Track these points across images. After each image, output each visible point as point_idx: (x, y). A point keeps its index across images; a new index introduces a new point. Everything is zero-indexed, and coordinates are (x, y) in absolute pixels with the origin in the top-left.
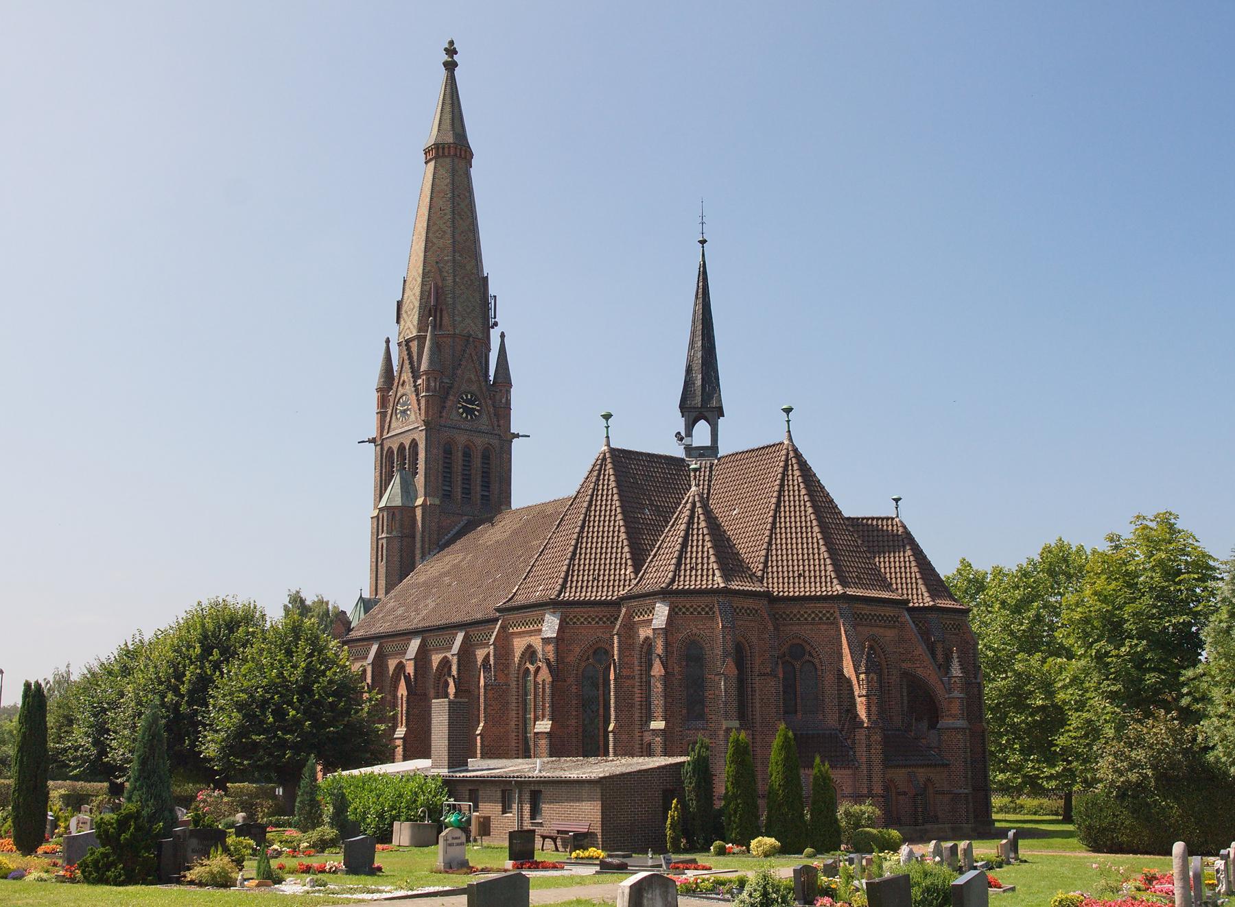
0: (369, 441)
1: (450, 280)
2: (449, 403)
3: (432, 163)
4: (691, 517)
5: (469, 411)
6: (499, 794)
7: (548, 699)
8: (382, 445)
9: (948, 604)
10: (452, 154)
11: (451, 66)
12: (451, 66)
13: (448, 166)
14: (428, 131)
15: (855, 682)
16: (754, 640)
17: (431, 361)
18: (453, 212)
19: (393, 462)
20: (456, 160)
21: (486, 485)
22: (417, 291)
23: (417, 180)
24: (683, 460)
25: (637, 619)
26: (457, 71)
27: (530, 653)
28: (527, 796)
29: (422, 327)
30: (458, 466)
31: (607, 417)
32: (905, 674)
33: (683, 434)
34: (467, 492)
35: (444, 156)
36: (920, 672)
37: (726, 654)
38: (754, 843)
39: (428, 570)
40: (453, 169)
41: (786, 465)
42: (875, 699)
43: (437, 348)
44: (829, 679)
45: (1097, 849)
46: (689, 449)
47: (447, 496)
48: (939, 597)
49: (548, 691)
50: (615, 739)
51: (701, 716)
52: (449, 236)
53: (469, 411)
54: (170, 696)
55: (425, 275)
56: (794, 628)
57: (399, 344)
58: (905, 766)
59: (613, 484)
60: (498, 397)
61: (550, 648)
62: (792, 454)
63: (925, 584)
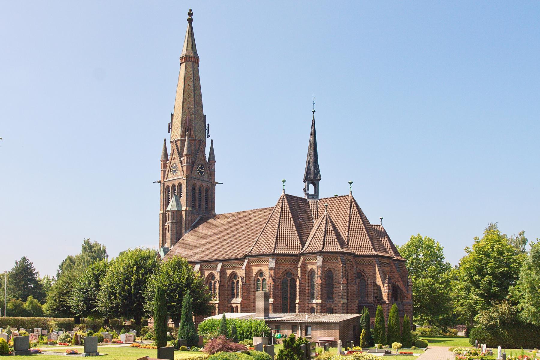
0: (158, 182)
1: (193, 116)
2: (194, 169)
3: (184, 64)
4: (326, 224)
6: (290, 327)
8: (164, 184)
9: (400, 258)
11: (190, 21)
12: (190, 21)
13: (191, 66)
18: (194, 87)
19: (169, 191)
25: (307, 262)
27: (261, 273)
28: (304, 328)
29: (183, 135)
30: (197, 195)
31: (284, 181)
34: (200, 205)
37: (343, 276)
38: (393, 345)
39: (190, 237)
40: (193, 68)
41: (351, 205)
44: (370, 285)
46: (308, 195)
47: (193, 207)
50: (299, 306)
51: (331, 298)
52: (192, 96)
54: (127, 287)
55: (183, 113)
57: (171, 142)
61: (272, 271)
62: (353, 200)
63: (393, 251)
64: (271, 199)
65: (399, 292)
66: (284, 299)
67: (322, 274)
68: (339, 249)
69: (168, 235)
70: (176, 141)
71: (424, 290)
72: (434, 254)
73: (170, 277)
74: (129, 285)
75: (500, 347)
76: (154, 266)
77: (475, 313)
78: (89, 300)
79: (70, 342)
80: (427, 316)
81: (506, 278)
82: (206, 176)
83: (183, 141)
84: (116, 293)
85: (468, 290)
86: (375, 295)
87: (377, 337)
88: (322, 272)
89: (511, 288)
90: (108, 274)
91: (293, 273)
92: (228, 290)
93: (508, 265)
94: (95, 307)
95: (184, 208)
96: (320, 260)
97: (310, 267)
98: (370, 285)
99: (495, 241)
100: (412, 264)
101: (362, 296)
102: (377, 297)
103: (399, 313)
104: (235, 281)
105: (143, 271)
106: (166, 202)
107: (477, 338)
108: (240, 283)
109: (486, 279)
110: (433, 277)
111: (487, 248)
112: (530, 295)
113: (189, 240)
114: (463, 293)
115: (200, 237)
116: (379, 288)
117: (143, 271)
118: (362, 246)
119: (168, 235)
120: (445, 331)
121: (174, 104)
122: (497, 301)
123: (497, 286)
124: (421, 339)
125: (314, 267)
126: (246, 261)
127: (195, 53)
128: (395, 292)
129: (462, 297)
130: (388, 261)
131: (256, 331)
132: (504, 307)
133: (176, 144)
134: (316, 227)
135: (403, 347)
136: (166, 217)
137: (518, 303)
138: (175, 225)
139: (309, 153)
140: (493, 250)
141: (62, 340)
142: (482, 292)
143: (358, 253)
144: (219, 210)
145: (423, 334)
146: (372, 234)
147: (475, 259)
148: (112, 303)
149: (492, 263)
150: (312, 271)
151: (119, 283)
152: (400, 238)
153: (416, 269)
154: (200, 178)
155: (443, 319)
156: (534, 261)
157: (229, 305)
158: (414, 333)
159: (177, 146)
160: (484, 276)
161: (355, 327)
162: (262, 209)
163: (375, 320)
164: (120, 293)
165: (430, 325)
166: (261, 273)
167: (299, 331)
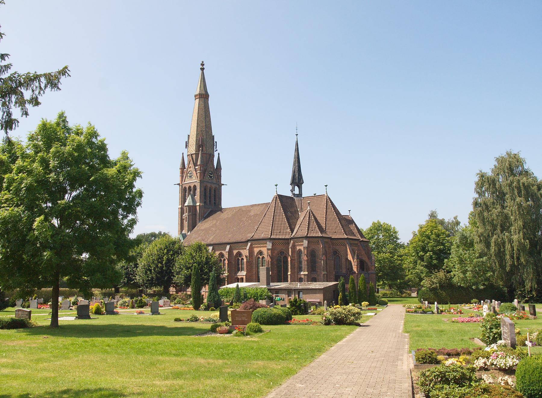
1: (205, 137)
4: (309, 216)
5: (211, 177)
9: (365, 240)
11: (202, 69)
12: (202, 69)
17: (201, 161)
19: (186, 191)
21: (215, 199)
22: (195, 139)
23: (193, 106)
28: (297, 293)
29: (197, 150)
30: (208, 194)
31: (276, 185)
34: (210, 201)
37: (323, 254)
38: (362, 303)
39: (202, 226)
44: (343, 260)
47: (205, 203)
52: (204, 122)
53: (211, 177)
54: (160, 265)
61: (270, 251)
64: (268, 197)
65: (365, 264)
66: (279, 271)
67: (307, 253)
68: (320, 235)
69: (186, 224)
70: (192, 155)
71: (384, 262)
72: (390, 234)
73: (193, 257)
74: (161, 263)
75: (436, 303)
76: (180, 249)
77: (421, 279)
78: (129, 274)
79: (128, 306)
80: (387, 281)
81: (442, 254)
82: (215, 179)
83: (197, 155)
84: (151, 270)
85: (415, 262)
86: (348, 268)
87: (350, 298)
88: (307, 251)
89: (446, 260)
90: (144, 255)
91: (285, 253)
92: (235, 264)
93: (443, 244)
94: (134, 280)
95: (198, 204)
96: (305, 243)
97: (298, 248)
98: (343, 260)
99: (433, 227)
100: (374, 243)
101: (339, 270)
102: (348, 269)
103: (366, 281)
104: (240, 258)
105: (171, 253)
106: (184, 200)
107: (423, 297)
108: (245, 260)
109: (428, 254)
110: (391, 253)
111: (428, 232)
112: (459, 266)
113: (203, 228)
114: (411, 265)
115: (211, 225)
116: (350, 262)
117: (171, 253)
118: (336, 232)
119: (186, 224)
120: (402, 293)
121: (190, 127)
122: (436, 271)
123: (436, 259)
124: (383, 299)
125: (302, 248)
126: (249, 244)
127: (206, 92)
128: (362, 265)
129: (412, 268)
130: (356, 242)
131: (261, 296)
132: (441, 274)
133: (192, 157)
134: (301, 218)
135: (370, 305)
136: (184, 210)
137: (451, 271)
139: (294, 164)
140: (432, 234)
141: (122, 305)
142: (425, 264)
143: (334, 237)
144: (224, 204)
145: (385, 295)
146: (343, 222)
147: (419, 240)
148: (148, 277)
149: (432, 243)
150: (300, 251)
151: (153, 262)
152: (364, 224)
153: (378, 247)
154: (210, 181)
155: (401, 283)
156: (460, 242)
157: (236, 277)
158: (377, 295)
159: (192, 159)
160: (426, 253)
161: (334, 291)
162: (259, 205)
163: (349, 286)
164: (154, 269)
165: (390, 288)
166: (261, 253)
167: (293, 296)
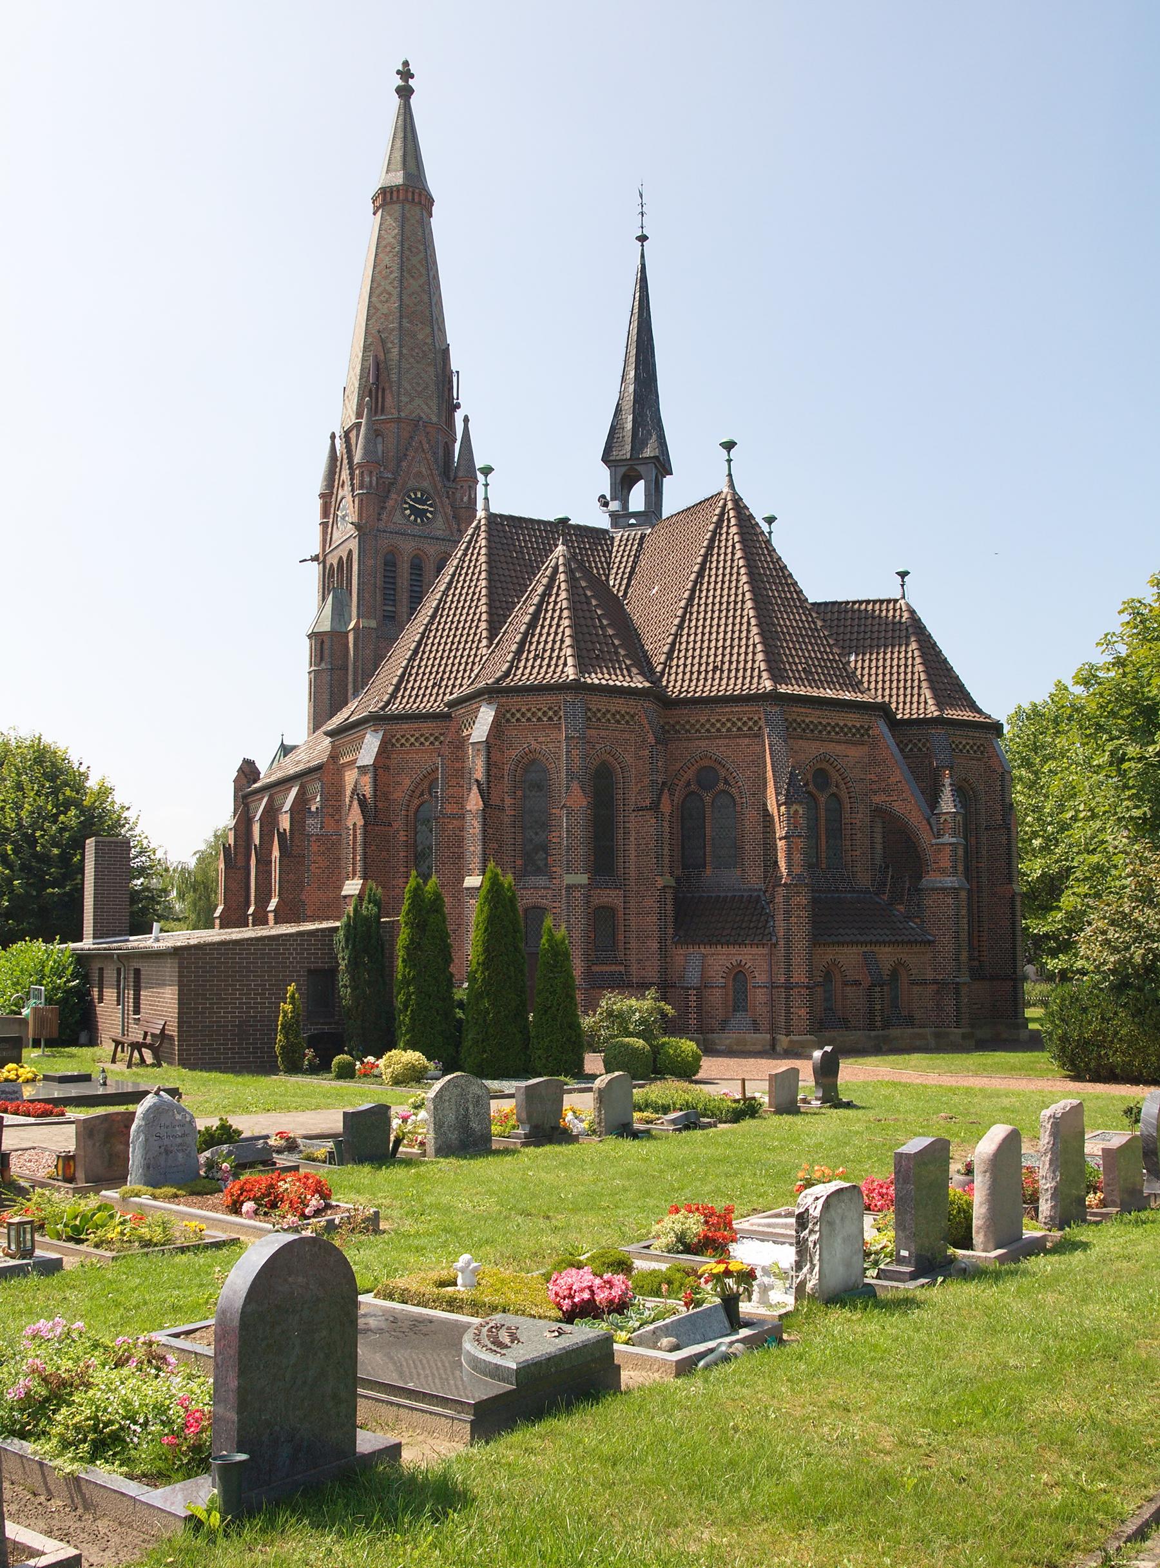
0: (312, 559)
4: (549, 587)
7: (359, 849)
8: (324, 562)
10: (407, 202)
11: (405, 92)
12: (405, 92)
13: (397, 214)
14: (376, 170)
15: (776, 819)
16: (629, 759)
18: (402, 270)
19: (334, 580)
20: (407, 206)
23: (360, 234)
24: (607, 531)
26: (414, 100)
32: (879, 812)
33: (608, 498)
35: (392, 202)
36: (898, 807)
42: (800, 843)
43: (375, 433)
44: (751, 816)
45: (1077, 1077)
46: (617, 519)
48: (952, 706)
49: (359, 838)
52: (395, 298)
56: (703, 743)
58: (857, 943)
59: (483, 559)
60: (458, 495)
62: (730, 505)
63: (932, 688)
82: (440, 522)
138: (326, 678)
